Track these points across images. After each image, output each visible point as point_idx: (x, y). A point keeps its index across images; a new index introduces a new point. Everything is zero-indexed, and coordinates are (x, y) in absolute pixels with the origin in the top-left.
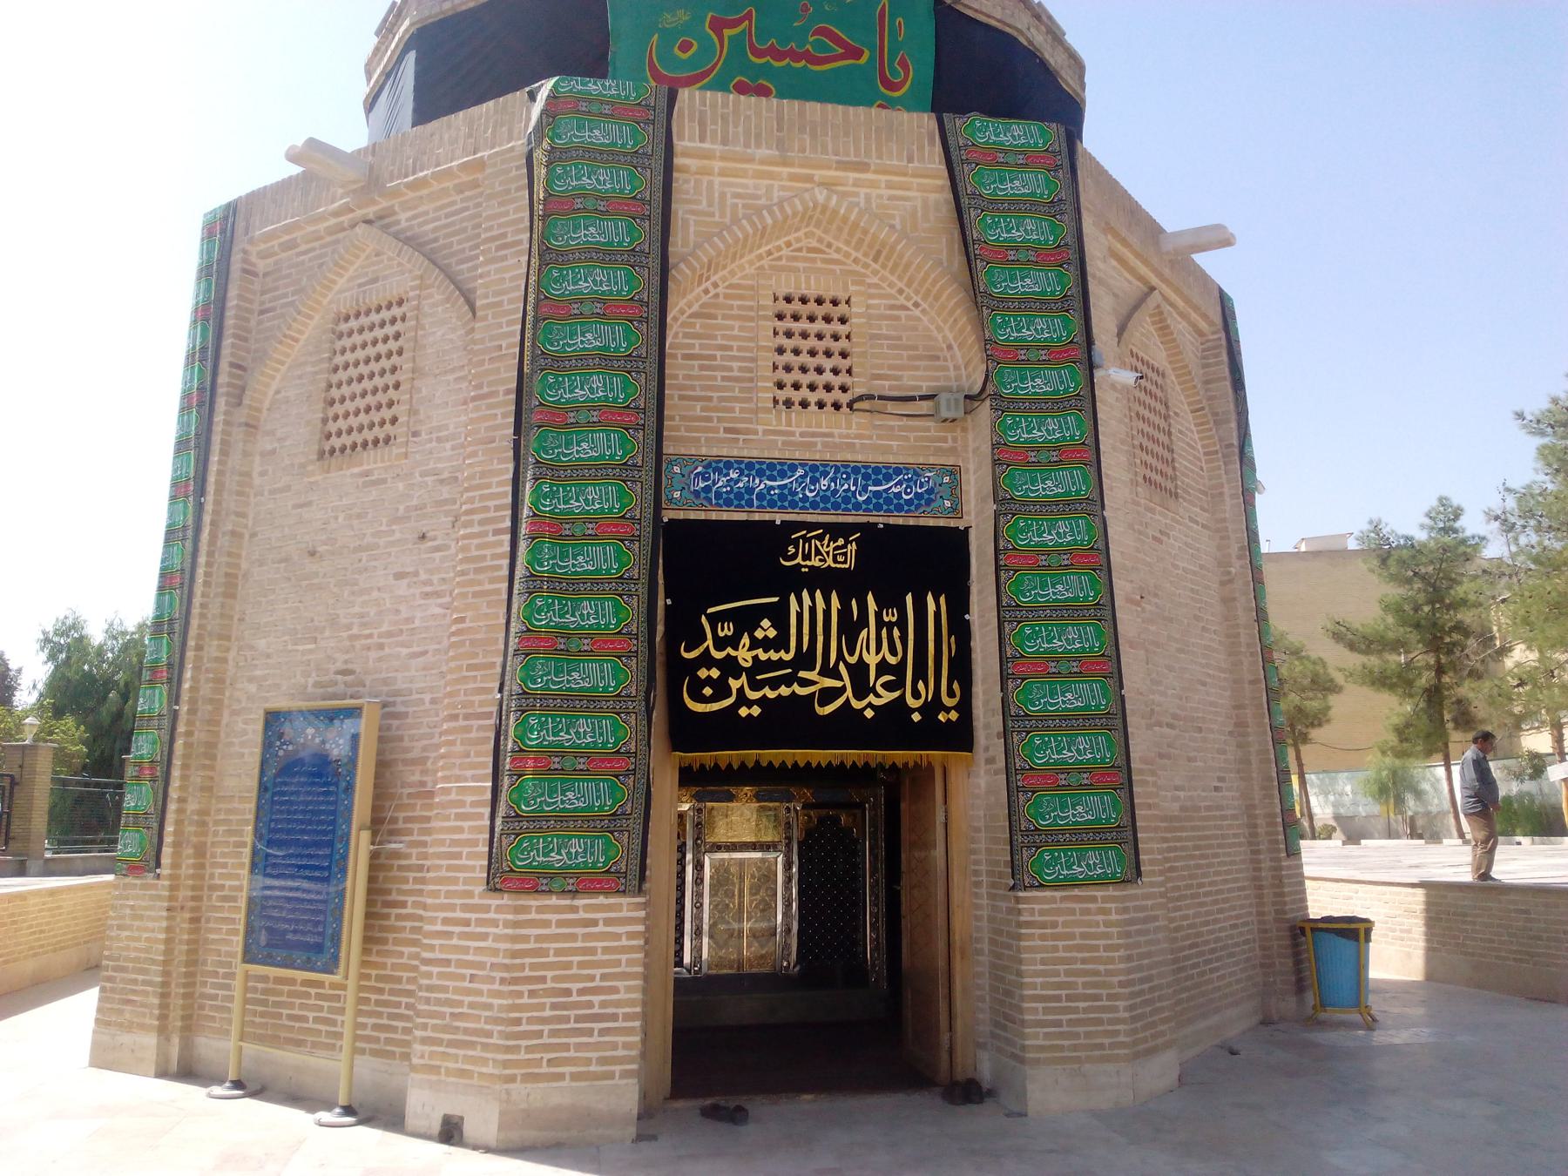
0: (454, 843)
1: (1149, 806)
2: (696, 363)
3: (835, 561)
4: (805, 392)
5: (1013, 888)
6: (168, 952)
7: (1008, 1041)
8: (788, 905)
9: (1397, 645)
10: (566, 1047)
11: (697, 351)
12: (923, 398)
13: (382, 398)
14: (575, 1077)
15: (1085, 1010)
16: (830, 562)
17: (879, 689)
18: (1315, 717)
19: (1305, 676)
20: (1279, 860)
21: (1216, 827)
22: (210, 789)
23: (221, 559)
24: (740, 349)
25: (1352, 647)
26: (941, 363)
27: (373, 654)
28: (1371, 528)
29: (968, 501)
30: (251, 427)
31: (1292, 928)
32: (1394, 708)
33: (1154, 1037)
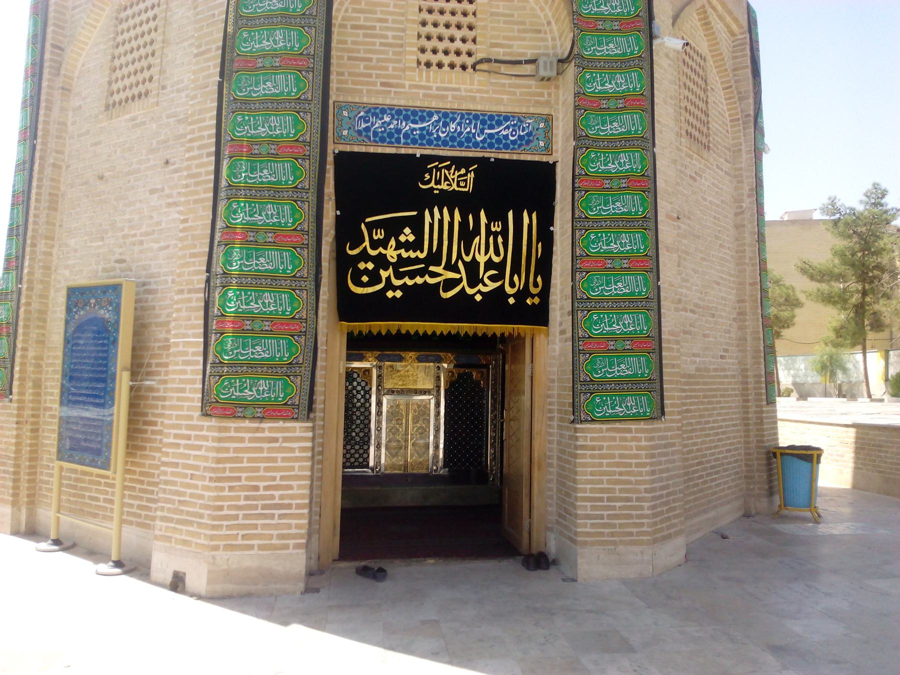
0: (182, 381)
1: (673, 366)
2: (360, 32)
3: (458, 186)
4: (440, 56)
5: (573, 422)
6: (18, 451)
7: (566, 527)
8: (437, 430)
9: (840, 277)
10: (255, 527)
11: (362, 23)
12: (528, 62)
13: (144, 63)
14: (261, 548)
15: (620, 508)
16: (455, 186)
17: (486, 281)
18: (786, 321)
19: (781, 297)
20: (761, 406)
21: (720, 383)
22: (43, 342)
23: (46, 183)
24: (394, 21)
25: (812, 278)
26: (542, 35)
27: (137, 248)
28: (830, 202)
29: (557, 142)
30: (66, 90)
31: (768, 453)
32: (835, 316)
33: (668, 528)
